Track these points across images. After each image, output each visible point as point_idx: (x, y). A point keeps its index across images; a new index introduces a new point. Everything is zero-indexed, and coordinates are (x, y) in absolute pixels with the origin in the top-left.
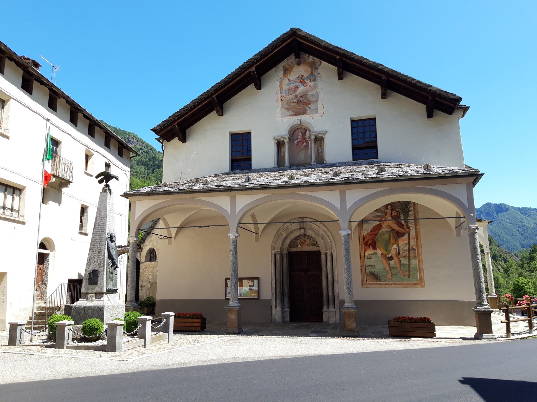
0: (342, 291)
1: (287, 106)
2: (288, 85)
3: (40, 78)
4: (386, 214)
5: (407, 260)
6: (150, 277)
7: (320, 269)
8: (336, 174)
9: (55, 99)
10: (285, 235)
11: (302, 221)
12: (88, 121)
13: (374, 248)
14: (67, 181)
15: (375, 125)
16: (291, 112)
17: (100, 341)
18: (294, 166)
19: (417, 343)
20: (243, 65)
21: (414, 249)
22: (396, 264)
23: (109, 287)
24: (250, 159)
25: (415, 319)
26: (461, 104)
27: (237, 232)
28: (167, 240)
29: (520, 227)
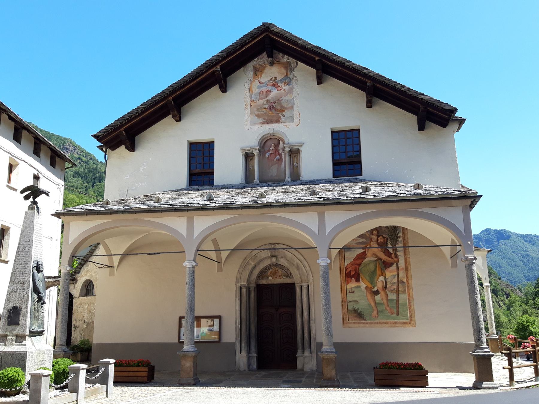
0: (319, 333)
1: (257, 113)
5: (395, 294)
6: (86, 315)
7: (294, 305)
8: (314, 193)
10: (253, 264)
11: (273, 248)
12: (13, 124)
13: (358, 280)
15: (359, 137)
16: (261, 120)
19: (407, 394)
20: (205, 63)
21: (403, 282)
23: (33, 328)
24: (213, 173)
27: (194, 261)
28: (108, 270)
29: (523, 257)
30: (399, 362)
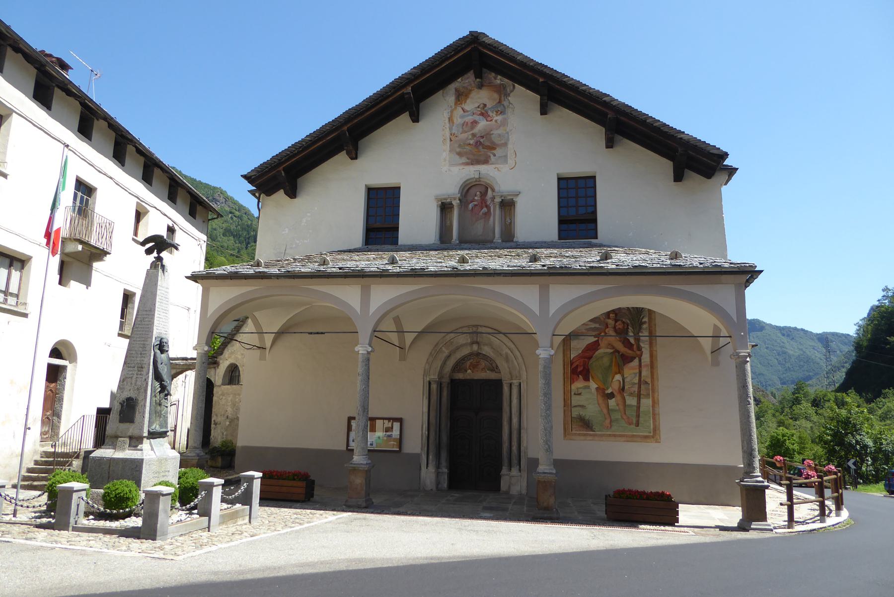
0: (534, 444)
1: (458, 150)
2: (462, 117)
3: (66, 85)
4: (607, 327)
5: (636, 399)
6: (229, 409)
7: (500, 409)
8: (534, 259)
9: (89, 120)
10: (446, 352)
11: (475, 332)
12: (142, 159)
13: (586, 379)
14: (103, 250)
15: (594, 187)
16: (464, 160)
17: (133, 518)
18: (466, 242)
19: (652, 535)
20: (392, 83)
21: (646, 383)
22: (618, 405)
23: (153, 427)
24: (396, 229)
25: (647, 494)
26: (725, 163)
27: (370, 345)
28: (258, 351)
29: (779, 354)
30: (640, 489)
